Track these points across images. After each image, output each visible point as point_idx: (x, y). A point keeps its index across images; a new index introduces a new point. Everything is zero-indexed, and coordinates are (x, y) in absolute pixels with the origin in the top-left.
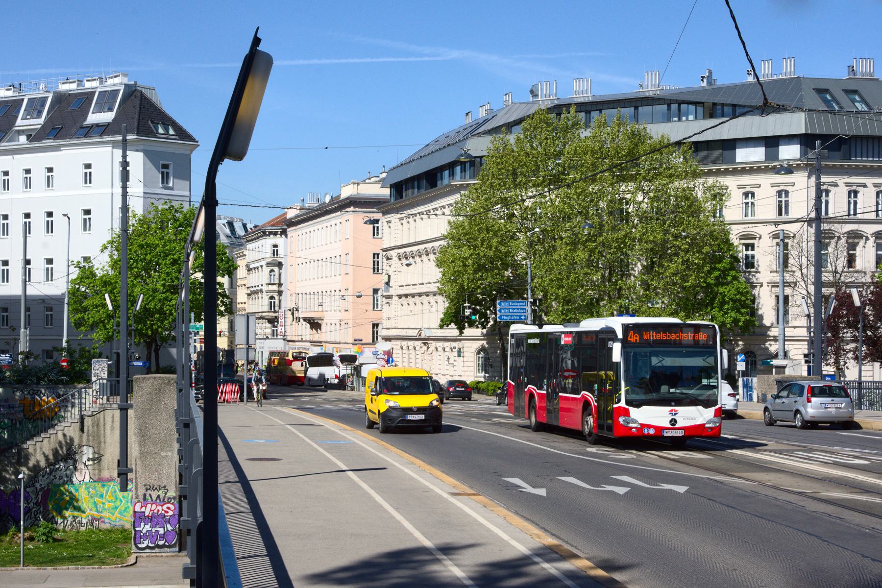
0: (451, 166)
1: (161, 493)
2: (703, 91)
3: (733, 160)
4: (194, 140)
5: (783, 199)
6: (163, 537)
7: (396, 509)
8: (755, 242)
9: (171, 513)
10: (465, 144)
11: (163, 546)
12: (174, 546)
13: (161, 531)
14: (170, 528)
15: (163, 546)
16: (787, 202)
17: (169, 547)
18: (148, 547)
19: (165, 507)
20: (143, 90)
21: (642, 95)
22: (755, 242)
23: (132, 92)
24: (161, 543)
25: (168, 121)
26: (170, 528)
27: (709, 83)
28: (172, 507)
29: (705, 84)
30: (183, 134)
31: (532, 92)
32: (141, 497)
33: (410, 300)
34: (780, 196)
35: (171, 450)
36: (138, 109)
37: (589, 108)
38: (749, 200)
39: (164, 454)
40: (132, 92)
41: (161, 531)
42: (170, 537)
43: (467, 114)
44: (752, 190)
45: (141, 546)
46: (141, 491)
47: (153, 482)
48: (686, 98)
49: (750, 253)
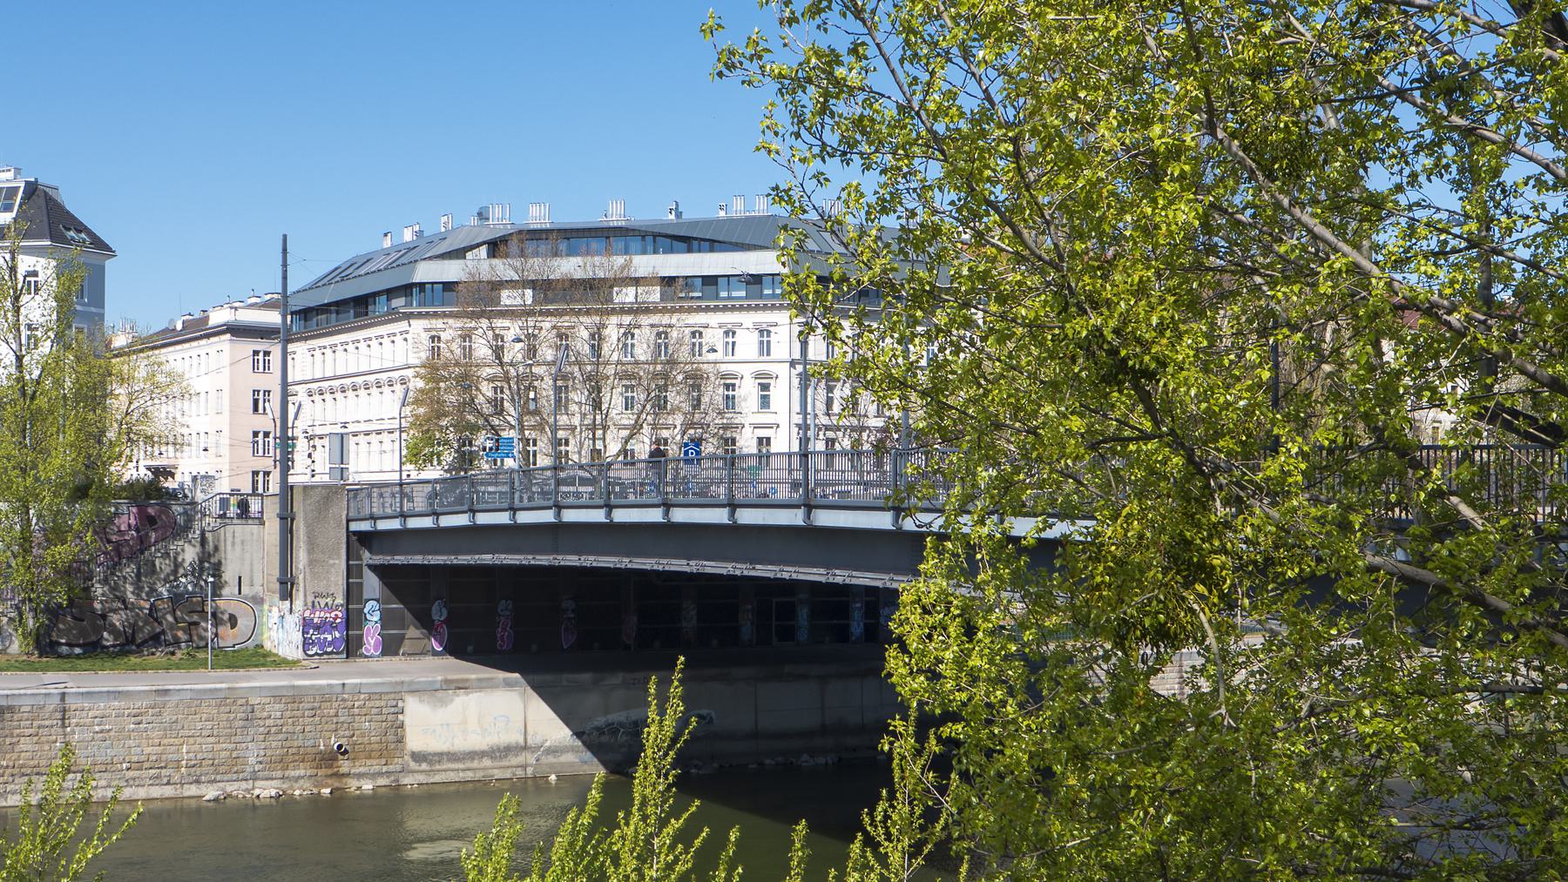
0: (391, 293)
1: (329, 600)
2: (670, 224)
3: (610, 300)
4: (110, 249)
5: (765, 339)
6: (330, 644)
7: (753, 561)
8: (772, 382)
9: (338, 620)
10: (413, 271)
11: (332, 653)
12: (341, 653)
13: (329, 638)
14: (338, 635)
15: (332, 653)
16: (769, 342)
17: (337, 653)
18: (316, 654)
19: (333, 615)
20: (47, 190)
21: (605, 225)
22: (772, 382)
23: (32, 189)
24: (329, 650)
25: (81, 228)
26: (338, 635)
27: (677, 216)
28: (340, 615)
29: (672, 217)
30: (99, 244)
31: (480, 214)
32: (310, 604)
33: (374, 438)
34: (762, 336)
35: (339, 558)
36: (45, 212)
37: (568, 235)
38: (436, 344)
39: (331, 562)
40: (32, 189)
41: (329, 638)
42: (338, 644)
43: (386, 235)
44: (502, 333)
45: (310, 653)
46: (310, 599)
47: (320, 590)
48: (663, 231)
49: (731, 393)
